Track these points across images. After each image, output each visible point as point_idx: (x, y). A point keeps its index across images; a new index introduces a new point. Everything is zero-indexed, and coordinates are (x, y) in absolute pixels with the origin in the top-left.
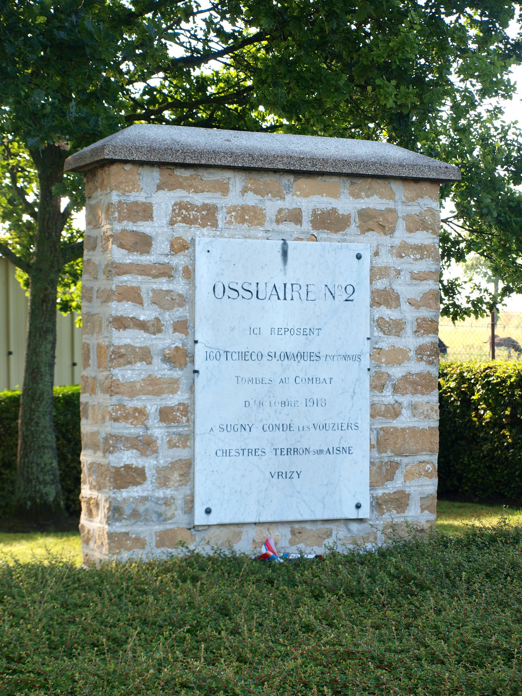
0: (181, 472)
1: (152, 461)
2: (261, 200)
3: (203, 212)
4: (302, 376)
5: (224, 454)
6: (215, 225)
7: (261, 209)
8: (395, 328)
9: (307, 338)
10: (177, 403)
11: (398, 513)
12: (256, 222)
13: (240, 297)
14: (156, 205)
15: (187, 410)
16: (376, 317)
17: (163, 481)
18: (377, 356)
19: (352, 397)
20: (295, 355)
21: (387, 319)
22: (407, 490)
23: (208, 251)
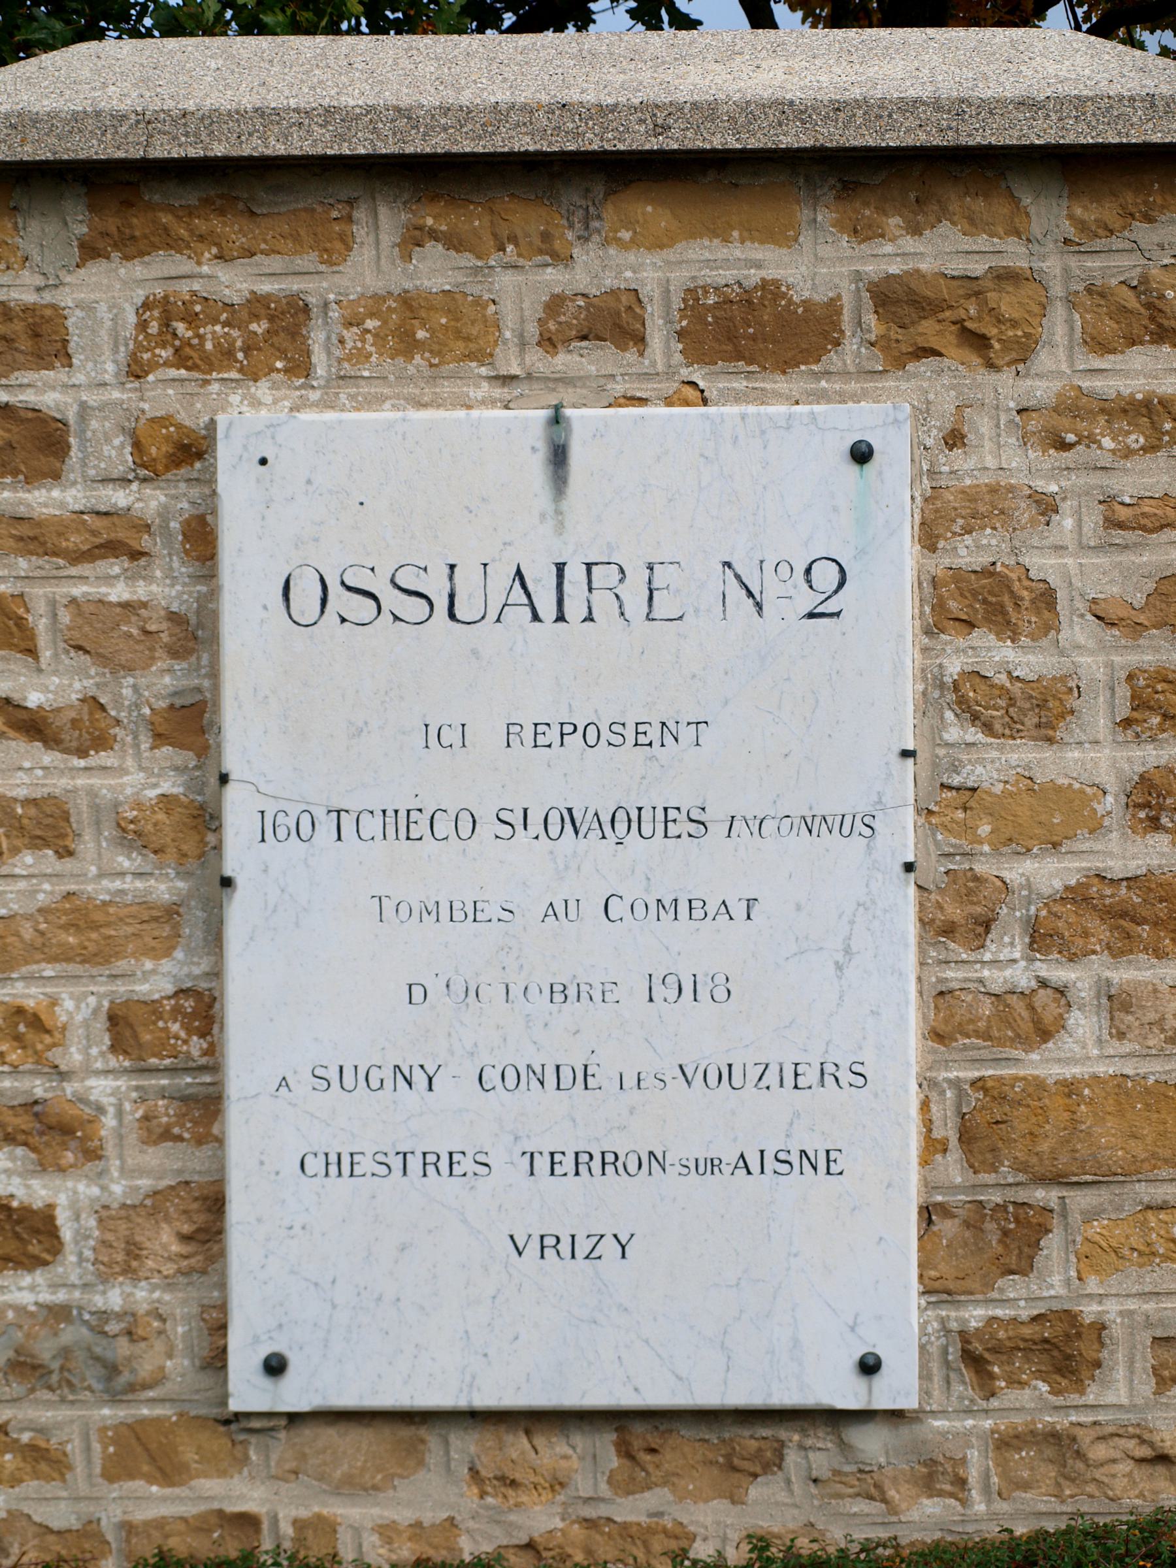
0: (186, 1228)
1: (81, 1187)
2: (476, 270)
3: (254, 327)
4: (632, 890)
5: (333, 1169)
6: (300, 368)
7: (478, 302)
8: (1042, 711)
9: (652, 758)
10: (170, 989)
11: (1055, 1392)
12: (459, 347)
13: (386, 617)
14: (79, 313)
15: (203, 1009)
16: (954, 667)
17: (125, 1259)
18: (960, 815)
19: (839, 967)
20: (606, 818)
21: (1002, 679)
22: (1089, 1311)
23: (263, 462)
